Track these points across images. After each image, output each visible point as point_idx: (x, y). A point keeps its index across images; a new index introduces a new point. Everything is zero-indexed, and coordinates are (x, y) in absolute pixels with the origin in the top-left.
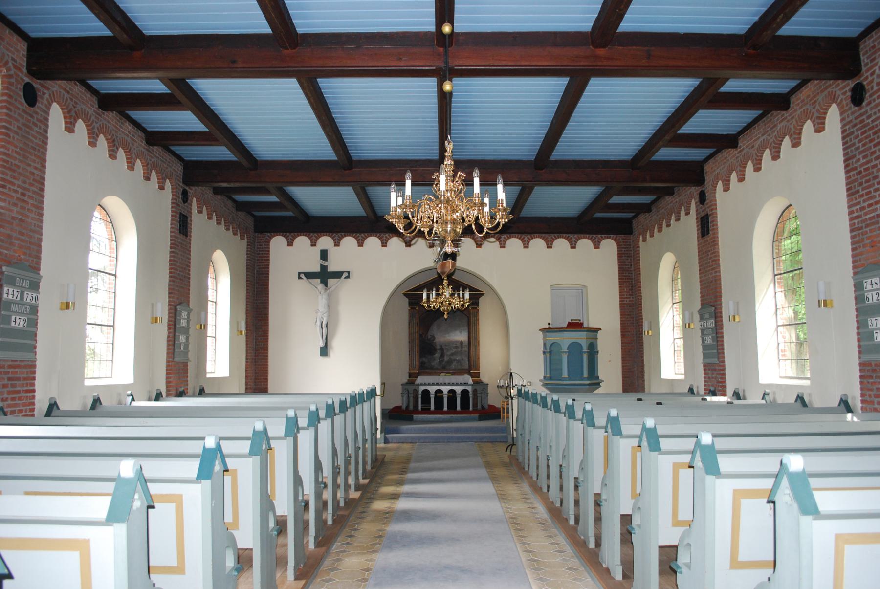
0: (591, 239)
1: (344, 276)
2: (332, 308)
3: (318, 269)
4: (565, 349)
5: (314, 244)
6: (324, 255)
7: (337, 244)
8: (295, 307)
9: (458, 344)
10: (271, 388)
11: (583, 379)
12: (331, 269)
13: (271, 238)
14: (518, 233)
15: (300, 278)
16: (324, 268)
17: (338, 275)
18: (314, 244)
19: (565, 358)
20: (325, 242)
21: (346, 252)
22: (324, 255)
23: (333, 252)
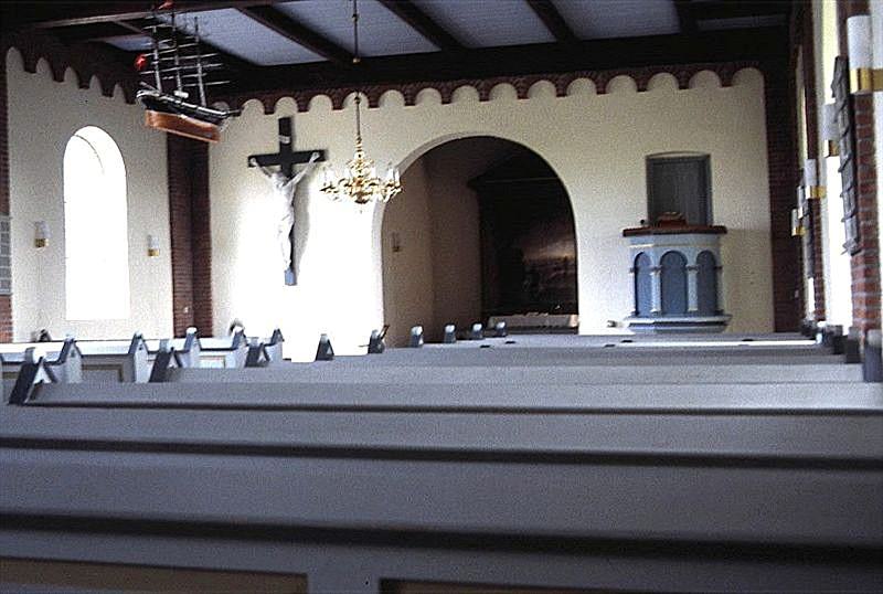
0: (594, 79)
1: (313, 159)
2: (297, 203)
3: (276, 149)
4: (691, 262)
5: (269, 111)
6: (286, 126)
7: (303, 108)
8: (251, 210)
9: (561, 265)
10: (215, 332)
11: (686, 313)
12: (299, 146)
13: (385, 91)
14: (547, 72)
15: (250, 166)
16: (286, 149)
17: (305, 156)
18: (269, 111)
19: (692, 276)
20: (286, 106)
21: (319, 122)
22: (286, 126)
23: (301, 122)
